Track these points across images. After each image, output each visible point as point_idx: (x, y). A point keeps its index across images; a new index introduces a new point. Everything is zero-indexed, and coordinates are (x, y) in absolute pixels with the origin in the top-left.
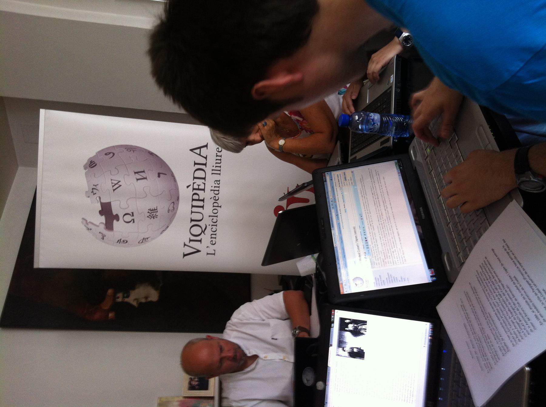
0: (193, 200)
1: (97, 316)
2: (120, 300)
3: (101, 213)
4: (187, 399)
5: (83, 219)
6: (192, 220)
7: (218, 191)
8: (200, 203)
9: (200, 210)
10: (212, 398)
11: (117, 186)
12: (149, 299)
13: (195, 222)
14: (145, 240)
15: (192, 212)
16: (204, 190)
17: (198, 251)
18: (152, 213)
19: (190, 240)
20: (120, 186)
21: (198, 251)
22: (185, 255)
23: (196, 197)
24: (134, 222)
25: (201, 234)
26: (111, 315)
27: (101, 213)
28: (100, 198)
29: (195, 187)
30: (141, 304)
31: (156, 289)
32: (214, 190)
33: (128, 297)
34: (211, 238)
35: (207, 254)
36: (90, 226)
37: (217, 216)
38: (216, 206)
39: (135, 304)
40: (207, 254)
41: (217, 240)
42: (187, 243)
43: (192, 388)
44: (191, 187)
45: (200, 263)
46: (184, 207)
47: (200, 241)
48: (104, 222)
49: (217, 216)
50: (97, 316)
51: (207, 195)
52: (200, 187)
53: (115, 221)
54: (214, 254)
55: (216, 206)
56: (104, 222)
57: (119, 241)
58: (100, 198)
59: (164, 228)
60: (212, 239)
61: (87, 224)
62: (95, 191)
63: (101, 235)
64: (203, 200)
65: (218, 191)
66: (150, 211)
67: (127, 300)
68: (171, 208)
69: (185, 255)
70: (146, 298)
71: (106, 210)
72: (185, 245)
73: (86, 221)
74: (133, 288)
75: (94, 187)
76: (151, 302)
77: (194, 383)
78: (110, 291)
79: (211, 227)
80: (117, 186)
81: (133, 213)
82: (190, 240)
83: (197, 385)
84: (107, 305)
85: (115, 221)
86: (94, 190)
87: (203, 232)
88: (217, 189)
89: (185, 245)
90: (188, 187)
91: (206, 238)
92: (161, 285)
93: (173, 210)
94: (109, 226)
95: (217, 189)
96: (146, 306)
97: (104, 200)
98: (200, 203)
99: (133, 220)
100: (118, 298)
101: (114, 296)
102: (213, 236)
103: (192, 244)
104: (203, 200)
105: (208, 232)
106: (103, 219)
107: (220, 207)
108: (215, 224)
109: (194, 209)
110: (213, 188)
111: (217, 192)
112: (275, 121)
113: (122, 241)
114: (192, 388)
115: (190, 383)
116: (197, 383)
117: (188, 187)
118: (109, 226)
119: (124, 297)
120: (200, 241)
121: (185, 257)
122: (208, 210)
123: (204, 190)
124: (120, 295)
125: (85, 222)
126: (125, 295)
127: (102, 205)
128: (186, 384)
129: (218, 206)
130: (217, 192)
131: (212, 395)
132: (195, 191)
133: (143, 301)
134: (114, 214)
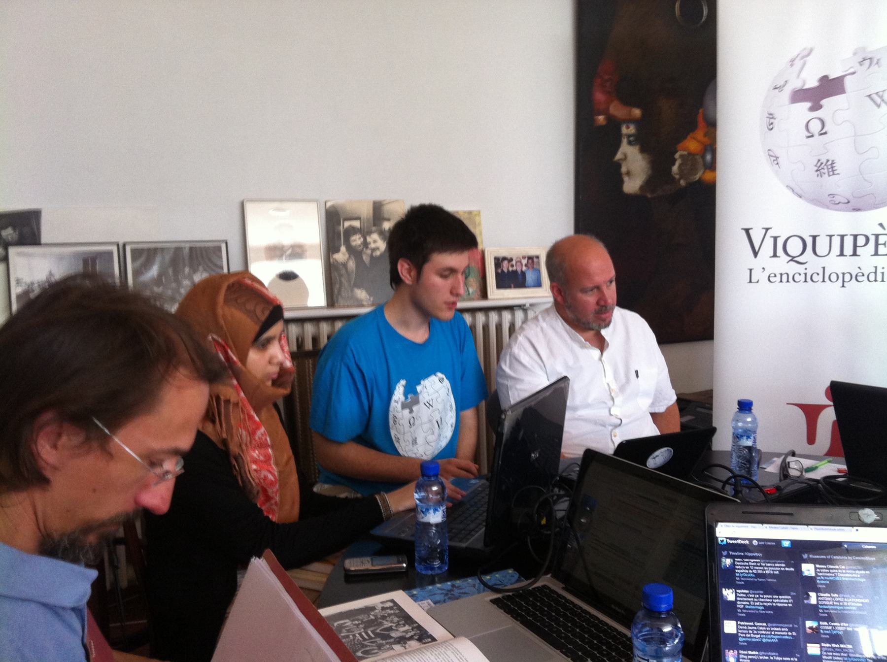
0: (855, 237)
1: (599, 96)
2: (624, 130)
3: (824, 79)
4: (479, 257)
5: (811, 51)
6: (814, 238)
7: (876, 280)
8: (848, 250)
9: (836, 249)
10: (484, 295)
11: (878, 100)
12: (626, 179)
13: (810, 244)
14: (775, 159)
15: (831, 236)
16: (876, 253)
17: (756, 254)
18: (826, 167)
19: (775, 239)
20: (879, 106)
21: (756, 254)
22: (747, 231)
23: (861, 241)
24: (809, 137)
25: (789, 256)
26: (601, 118)
27: (824, 79)
28: (854, 73)
29: (859, 237)
30: (618, 165)
31: (642, 188)
32: (876, 273)
33: (630, 143)
34: (781, 275)
35: (751, 270)
36: (798, 63)
37: (824, 281)
38: (844, 279)
39: (619, 156)
40: (751, 270)
41: (778, 284)
42: (770, 233)
43: (498, 262)
44: (879, 230)
45: (733, 260)
46: (841, 222)
47: (775, 255)
48: (807, 86)
49: (824, 281)
50: (599, 96)
51: (866, 259)
52: (881, 248)
53: (808, 105)
54: (750, 282)
55: (844, 279)
56: (806, 87)
57: (771, 116)
58: (854, 73)
59: (797, 190)
60: (779, 276)
61: (803, 58)
62: (867, 62)
63: (782, 83)
64: (855, 254)
65: (876, 280)
66: (830, 163)
67: (625, 141)
68: (837, 199)
69: (747, 231)
70: (628, 173)
71: (830, 87)
72: (767, 229)
73: (809, 54)
74: (642, 151)
75: (875, 62)
76: (621, 182)
77: (505, 266)
78: (637, 112)
79: (802, 271)
80: (878, 100)
81: (825, 133)
82: (775, 239)
83: (502, 271)
84: (617, 110)
85: (808, 105)
86: (868, 61)
87: (793, 259)
88: (879, 278)
89: (767, 229)
90: (881, 225)
91: (782, 264)
92: (649, 196)
93: (833, 202)
94: (799, 95)
95: (879, 278)
96: (615, 175)
97: (848, 82)
98: (848, 250)
99: (812, 136)
100: (628, 128)
101: (629, 121)
102: (785, 278)
103: (769, 242)
104: (855, 254)
105: (793, 268)
106: (812, 82)
107: (843, 286)
108: (809, 278)
109: (836, 241)
110: (879, 271)
111: (872, 277)
112: (399, 454)
113: (772, 121)
114: (498, 262)
115: (504, 259)
116: (505, 270)
117: (881, 225)
118: (799, 95)
119: (629, 136)
120: (775, 255)
121: (744, 232)
122: (836, 264)
123: (876, 253)
124: (632, 130)
125: (806, 52)
126: (631, 139)
127: (839, 81)
128: (502, 253)
129: (844, 281)
130: (872, 277)
131: (489, 296)
132: (872, 239)
133: (624, 169)
134: (824, 102)
